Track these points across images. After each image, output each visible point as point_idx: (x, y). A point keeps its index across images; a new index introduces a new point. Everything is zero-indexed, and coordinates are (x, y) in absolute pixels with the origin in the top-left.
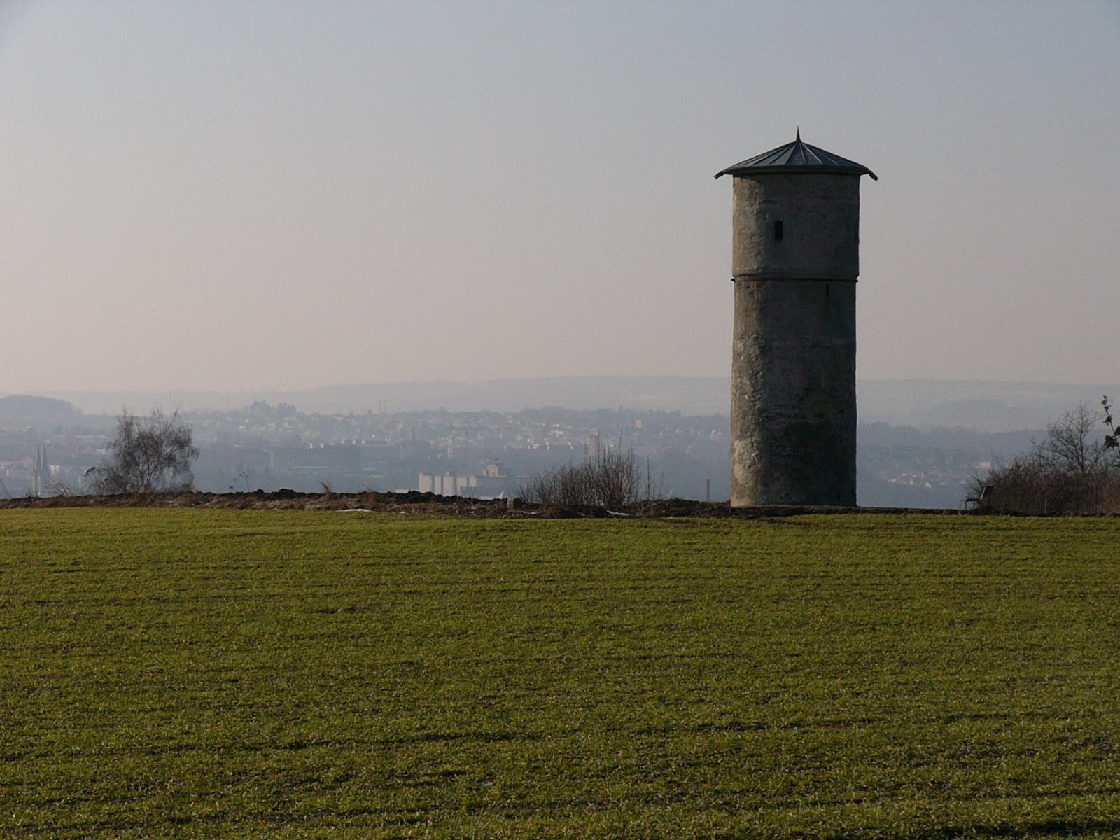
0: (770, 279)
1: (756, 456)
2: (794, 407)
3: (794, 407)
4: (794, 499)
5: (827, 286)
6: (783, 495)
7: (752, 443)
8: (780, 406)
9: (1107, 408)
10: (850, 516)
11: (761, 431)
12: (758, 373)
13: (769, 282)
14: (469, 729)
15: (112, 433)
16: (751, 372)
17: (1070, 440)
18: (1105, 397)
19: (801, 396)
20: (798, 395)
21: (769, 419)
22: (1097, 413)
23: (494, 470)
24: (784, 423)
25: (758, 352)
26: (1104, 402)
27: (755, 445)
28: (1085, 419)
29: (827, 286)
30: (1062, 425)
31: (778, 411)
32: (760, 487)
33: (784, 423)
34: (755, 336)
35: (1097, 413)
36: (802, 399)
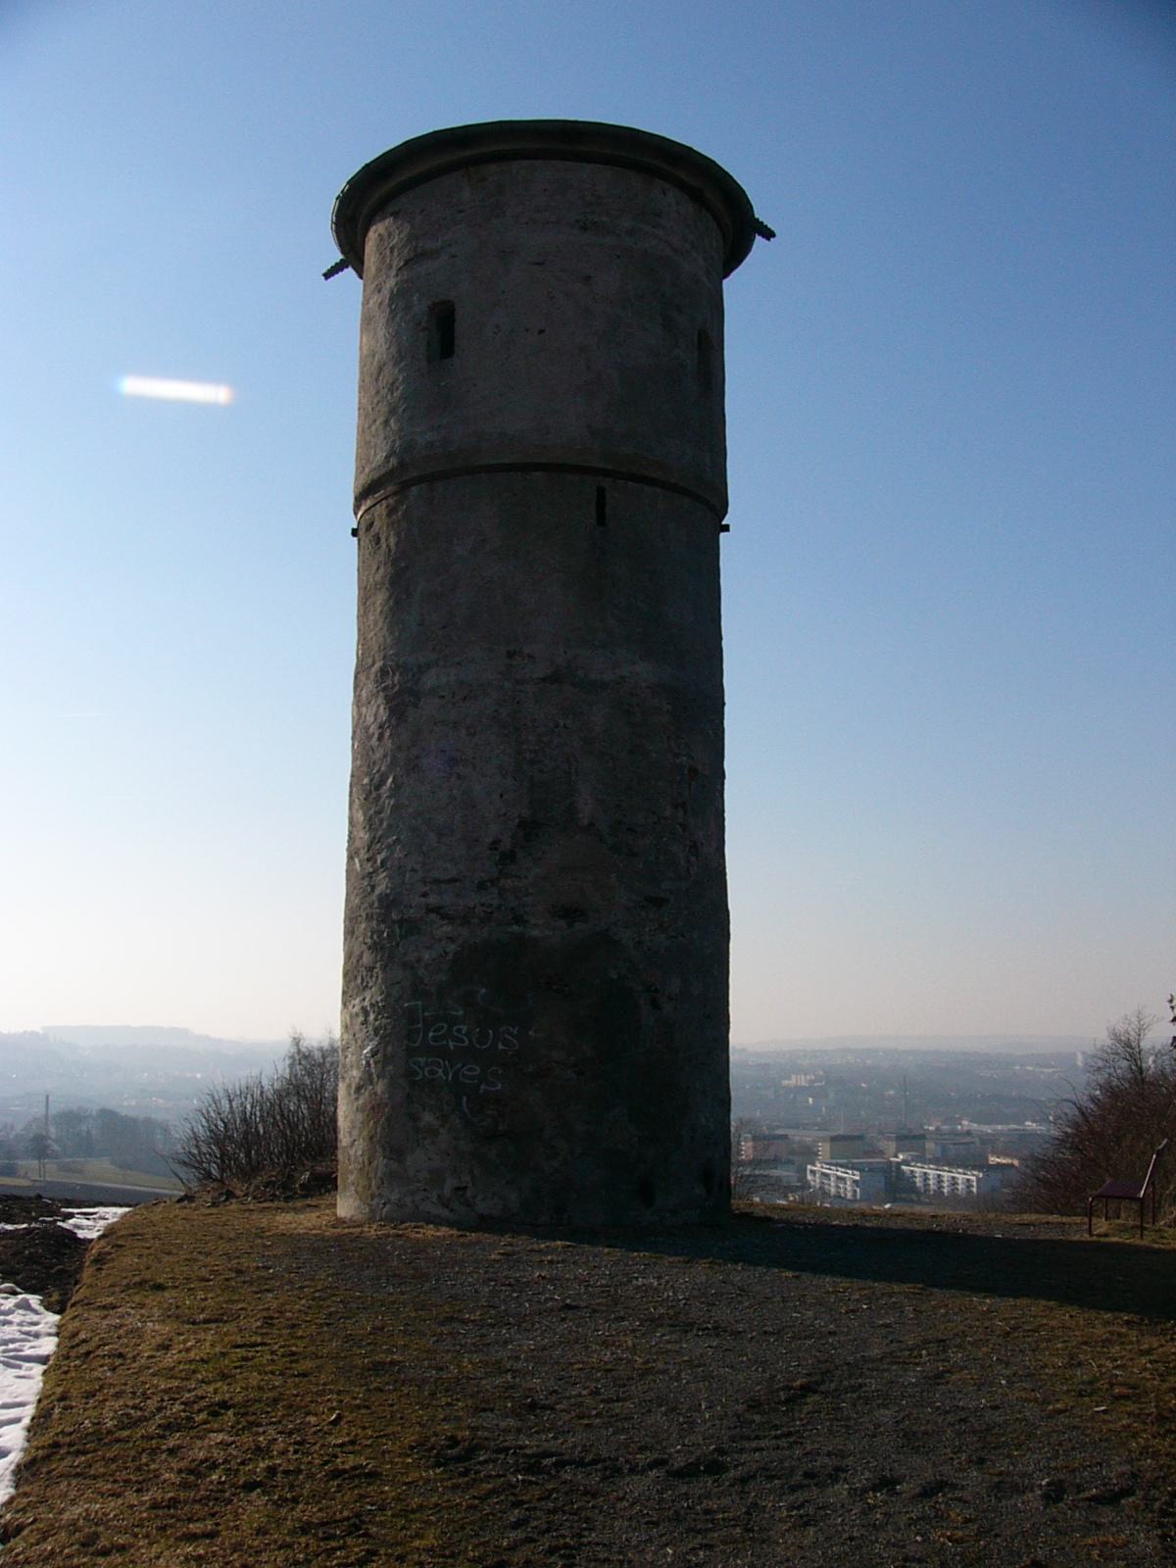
0: (420, 480)
1: (374, 1053)
2: (481, 886)
3: (481, 886)
4: (482, 1207)
5: (601, 493)
6: (447, 1191)
7: (366, 1012)
8: (437, 881)
9: (1173, 1008)
10: (676, 1280)
11: (384, 968)
12: (382, 782)
13: (414, 490)
14: (515, 1365)
15: (287, 1048)
16: (366, 781)
17: (1128, 1045)
18: (1172, 995)
19: (506, 844)
20: (495, 845)
21: (410, 927)
22: (1155, 1016)
23: (821, 1073)
24: (451, 940)
25: (383, 715)
26: (1171, 1001)
27: (372, 1017)
28: (1142, 1023)
29: (601, 493)
30: (1121, 1028)
31: (433, 900)
32: (380, 1161)
33: (451, 940)
34: (378, 665)
35: (1155, 1016)
36: (509, 857)
